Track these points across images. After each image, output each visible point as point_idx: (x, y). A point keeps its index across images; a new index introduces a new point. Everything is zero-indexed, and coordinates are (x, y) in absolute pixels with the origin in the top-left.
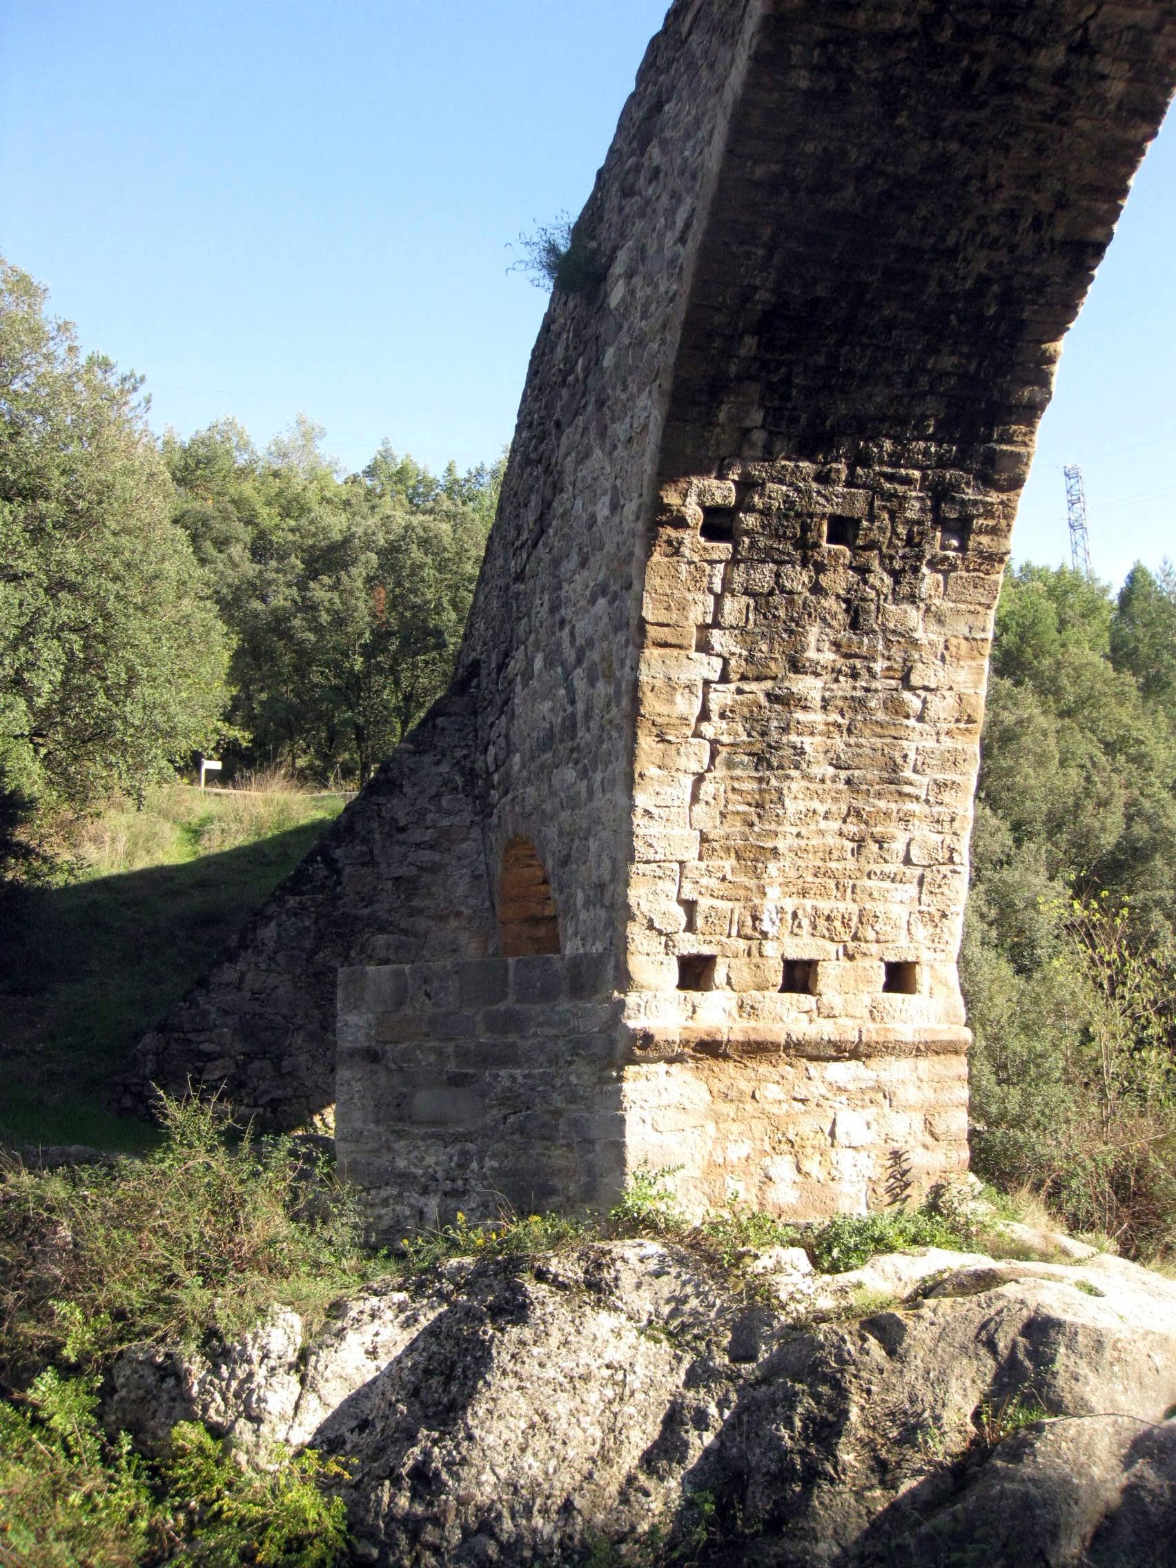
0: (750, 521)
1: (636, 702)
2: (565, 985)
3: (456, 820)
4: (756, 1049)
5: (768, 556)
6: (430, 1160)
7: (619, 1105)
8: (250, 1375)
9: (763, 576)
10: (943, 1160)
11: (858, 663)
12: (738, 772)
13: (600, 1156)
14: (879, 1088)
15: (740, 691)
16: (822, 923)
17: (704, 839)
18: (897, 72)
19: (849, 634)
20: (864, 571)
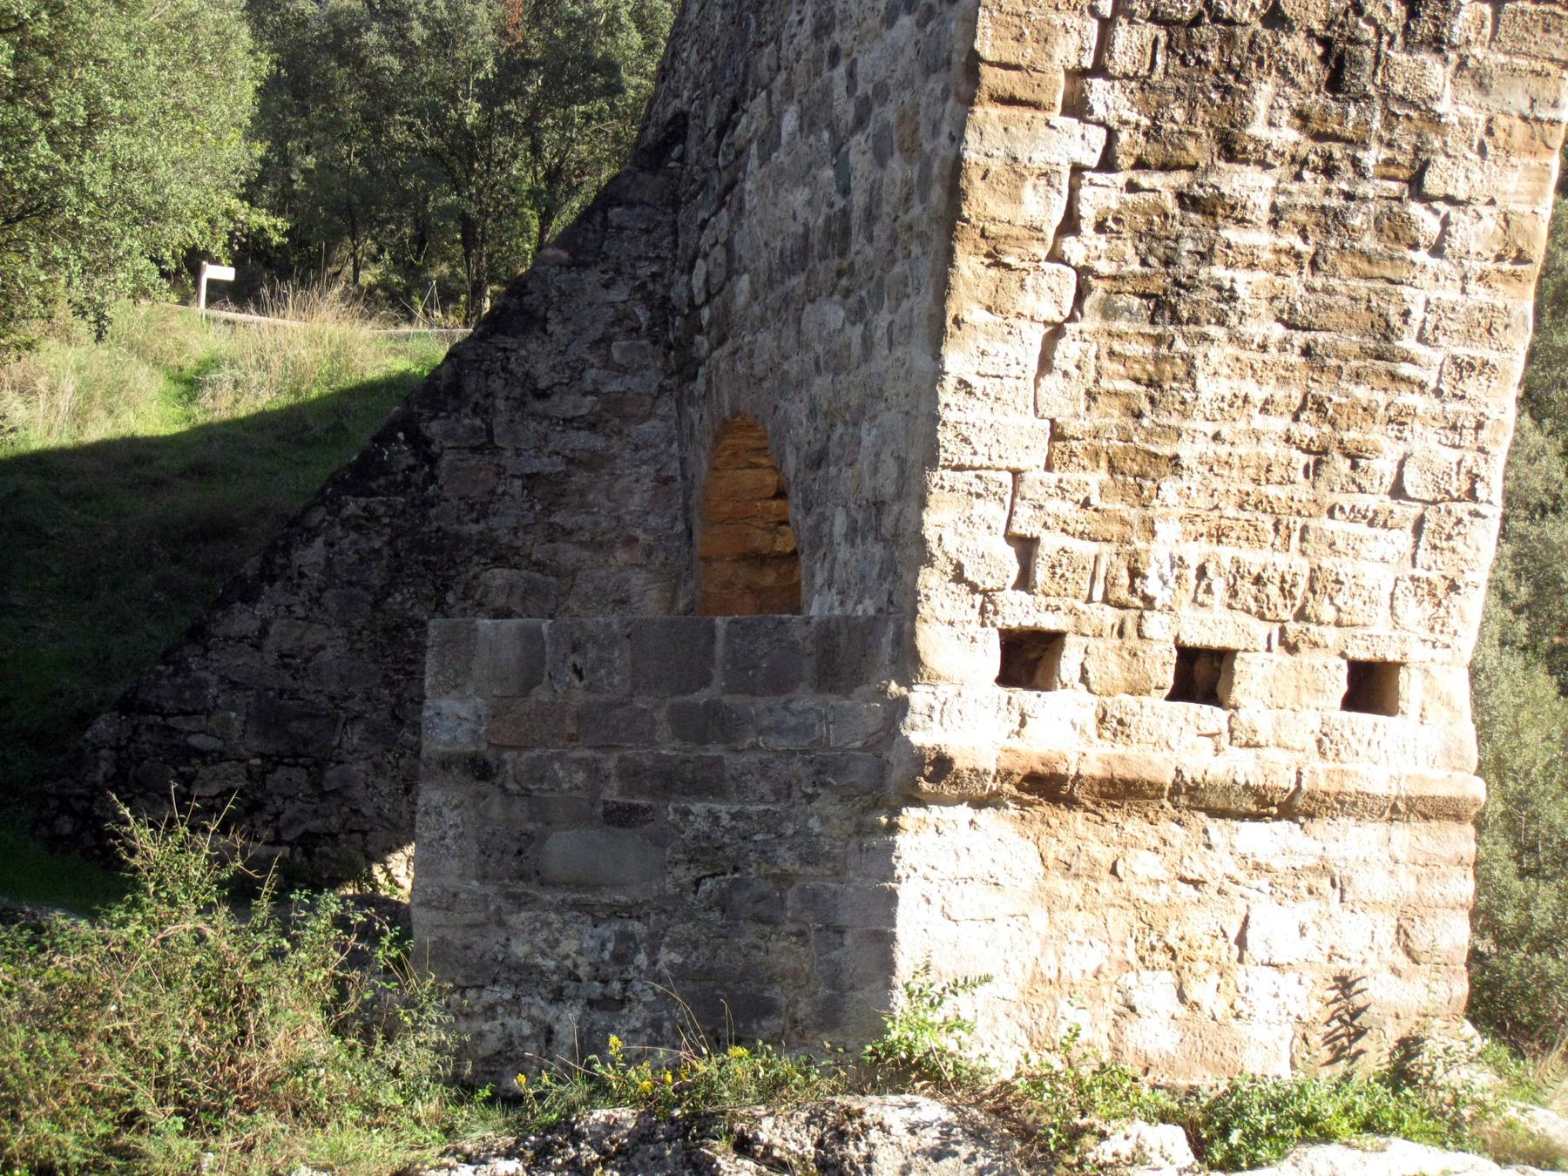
1: (956, 195)
2: (808, 667)
3: (633, 382)
4: (1122, 793)
6: (569, 946)
7: (889, 872)
10: (1421, 996)
11: (1337, 150)
12: (1121, 325)
14: (1323, 870)
15: (1132, 187)
16: (1246, 588)
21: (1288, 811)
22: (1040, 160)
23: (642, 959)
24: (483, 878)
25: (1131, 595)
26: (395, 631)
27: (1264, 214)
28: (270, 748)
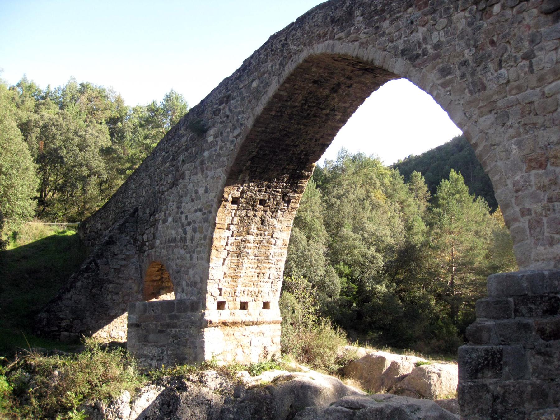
0: (242, 200)
1: (211, 242)
2: (189, 308)
3: (131, 253)
4: (235, 324)
5: (245, 208)
6: (153, 352)
7: (203, 338)
8: (119, 408)
9: (243, 213)
10: (275, 349)
11: (262, 232)
12: (233, 258)
13: (198, 350)
14: (261, 332)
15: (235, 239)
16: (250, 293)
17: (225, 274)
18: (294, 113)
19: (261, 226)
20: (265, 211)
21: (256, 324)
22: (223, 237)
23: (165, 353)
24: (139, 342)
25: (234, 295)
26: (94, 296)
27: (252, 241)
28: (73, 317)
